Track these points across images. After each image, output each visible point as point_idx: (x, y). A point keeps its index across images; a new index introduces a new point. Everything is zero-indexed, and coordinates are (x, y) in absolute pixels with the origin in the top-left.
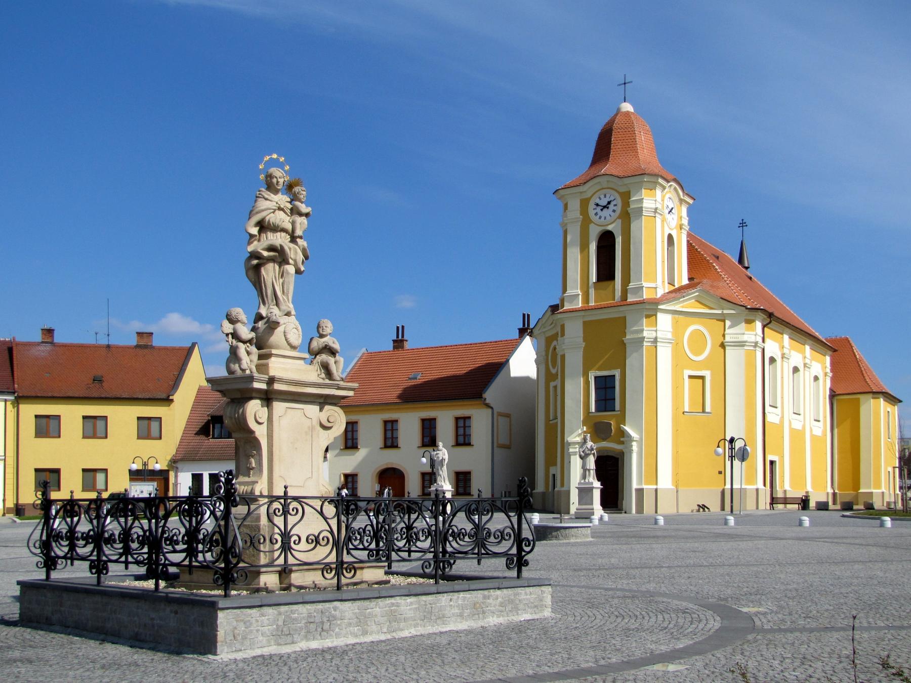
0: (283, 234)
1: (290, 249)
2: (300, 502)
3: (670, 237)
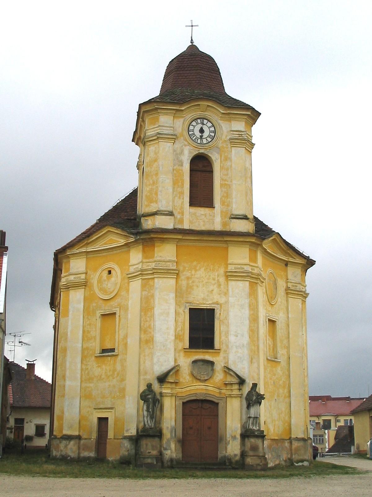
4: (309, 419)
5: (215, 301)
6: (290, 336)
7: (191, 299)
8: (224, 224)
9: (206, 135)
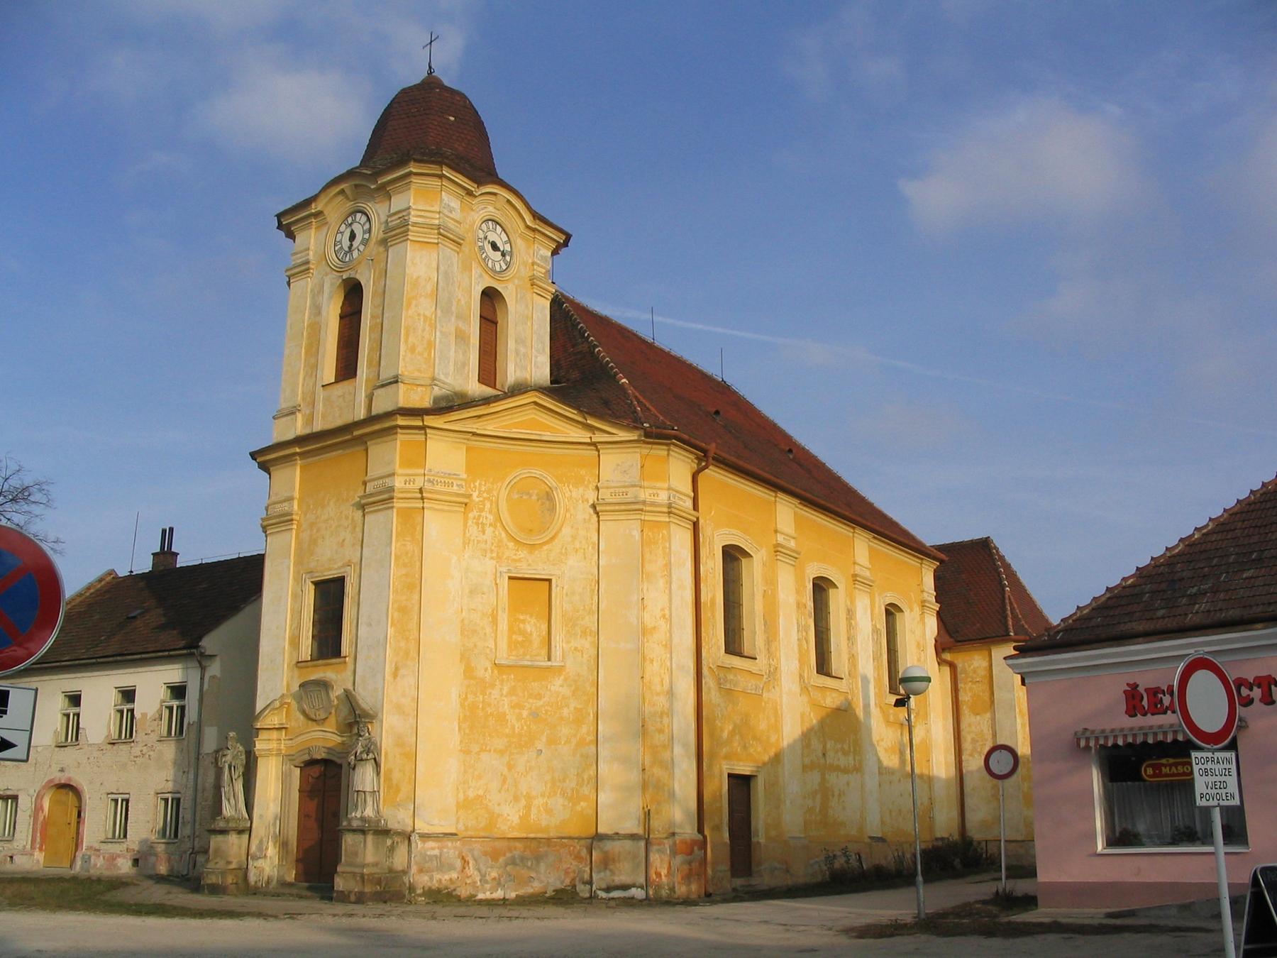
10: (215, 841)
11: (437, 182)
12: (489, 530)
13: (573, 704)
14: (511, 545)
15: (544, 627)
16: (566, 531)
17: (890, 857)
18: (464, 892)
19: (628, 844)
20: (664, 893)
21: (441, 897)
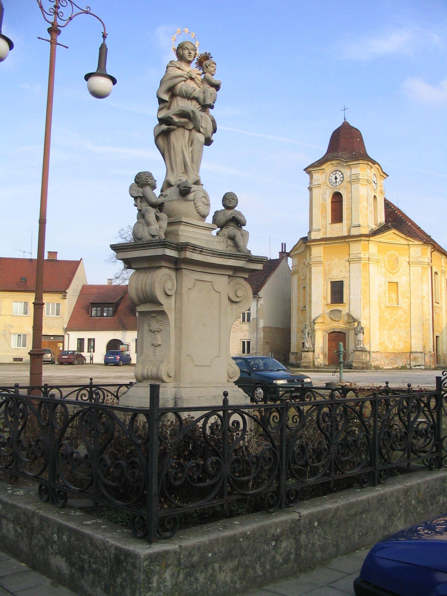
0: (194, 102)
1: (202, 117)
2: (241, 414)
3: (375, 197)
4: (246, 341)
5: (343, 276)
6: (411, 290)
7: (330, 277)
8: (349, 231)
9: (338, 180)
10: (304, 354)
11: (366, 166)
12: (383, 269)
13: (405, 317)
14: (388, 273)
15: (396, 296)
16: (401, 269)
17: (140, 374)
18: (381, 367)
19: (420, 354)
20: (428, 367)
21: (377, 368)
